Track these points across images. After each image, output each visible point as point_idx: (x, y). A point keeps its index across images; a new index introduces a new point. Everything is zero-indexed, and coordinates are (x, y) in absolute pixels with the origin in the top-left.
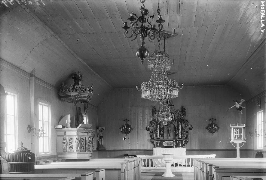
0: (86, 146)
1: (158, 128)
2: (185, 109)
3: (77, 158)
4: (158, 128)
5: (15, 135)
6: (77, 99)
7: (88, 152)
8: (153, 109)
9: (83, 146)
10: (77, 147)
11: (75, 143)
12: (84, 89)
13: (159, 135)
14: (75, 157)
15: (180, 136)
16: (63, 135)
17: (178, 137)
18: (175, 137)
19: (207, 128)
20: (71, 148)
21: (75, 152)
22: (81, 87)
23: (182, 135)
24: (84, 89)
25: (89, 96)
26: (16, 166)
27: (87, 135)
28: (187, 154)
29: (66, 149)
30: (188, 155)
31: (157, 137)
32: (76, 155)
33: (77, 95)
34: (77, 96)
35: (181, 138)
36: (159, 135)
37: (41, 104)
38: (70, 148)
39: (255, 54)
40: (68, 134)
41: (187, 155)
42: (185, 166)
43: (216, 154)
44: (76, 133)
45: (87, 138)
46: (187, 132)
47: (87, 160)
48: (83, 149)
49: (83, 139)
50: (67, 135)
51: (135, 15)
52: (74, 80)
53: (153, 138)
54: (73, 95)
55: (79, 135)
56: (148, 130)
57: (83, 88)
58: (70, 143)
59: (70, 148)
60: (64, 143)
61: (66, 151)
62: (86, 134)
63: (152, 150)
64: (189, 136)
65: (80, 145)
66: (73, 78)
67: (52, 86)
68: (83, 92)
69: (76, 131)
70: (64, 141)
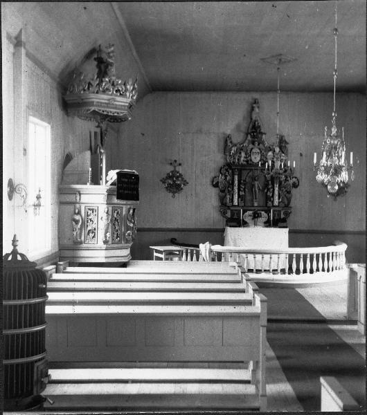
0: (123, 230)
1: (236, 182)
2: (287, 143)
3: (103, 260)
4: (236, 182)
8: (226, 140)
10: (106, 232)
11: (101, 223)
13: (236, 197)
14: (100, 256)
15: (277, 200)
17: (273, 202)
18: (267, 203)
19: (163, 181)
20: (91, 234)
21: (101, 244)
23: (279, 199)
26: (22, 372)
28: (291, 245)
29: (80, 238)
30: (292, 247)
31: (232, 200)
33: (106, 101)
34: (105, 103)
35: (278, 206)
36: (236, 197)
37: (33, 123)
38: (88, 234)
41: (290, 246)
42: (283, 271)
43: (345, 242)
46: (289, 192)
47: (124, 265)
52: (96, 63)
53: (226, 203)
54: (98, 102)
56: (216, 186)
58: (90, 223)
60: (77, 222)
61: (81, 243)
63: (223, 231)
64: (293, 200)
65: (110, 227)
66: (95, 59)
67: (52, 77)
68: (120, 94)
70: (77, 217)
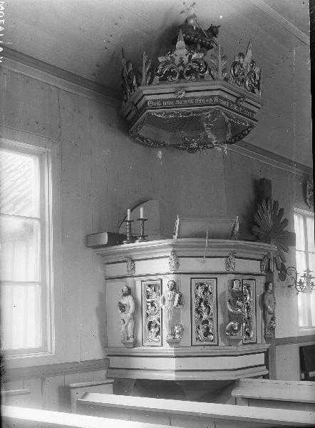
3: (171, 377)
5: (43, 284)
6: (172, 113)
7: (233, 348)
9: (206, 322)
12: (199, 64)
14: (166, 369)
16: (125, 273)
22: (186, 60)
24: (199, 64)
25: (234, 99)
27: (223, 269)
32: (172, 364)
38: (149, 328)
39: (94, 383)
40: (142, 268)
44: (167, 260)
45: (223, 282)
48: (207, 333)
49: (206, 289)
50: (138, 272)
51: (265, 377)
55: (181, 269)
57: (195, 61)
59: (149, 328)
61: (135, 344)
62: (218, 265)
67: (70, 76)
69: (169, 254)
